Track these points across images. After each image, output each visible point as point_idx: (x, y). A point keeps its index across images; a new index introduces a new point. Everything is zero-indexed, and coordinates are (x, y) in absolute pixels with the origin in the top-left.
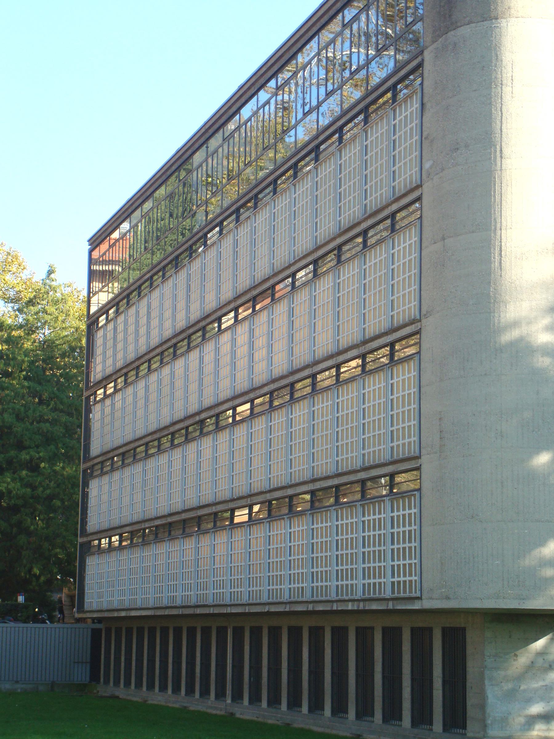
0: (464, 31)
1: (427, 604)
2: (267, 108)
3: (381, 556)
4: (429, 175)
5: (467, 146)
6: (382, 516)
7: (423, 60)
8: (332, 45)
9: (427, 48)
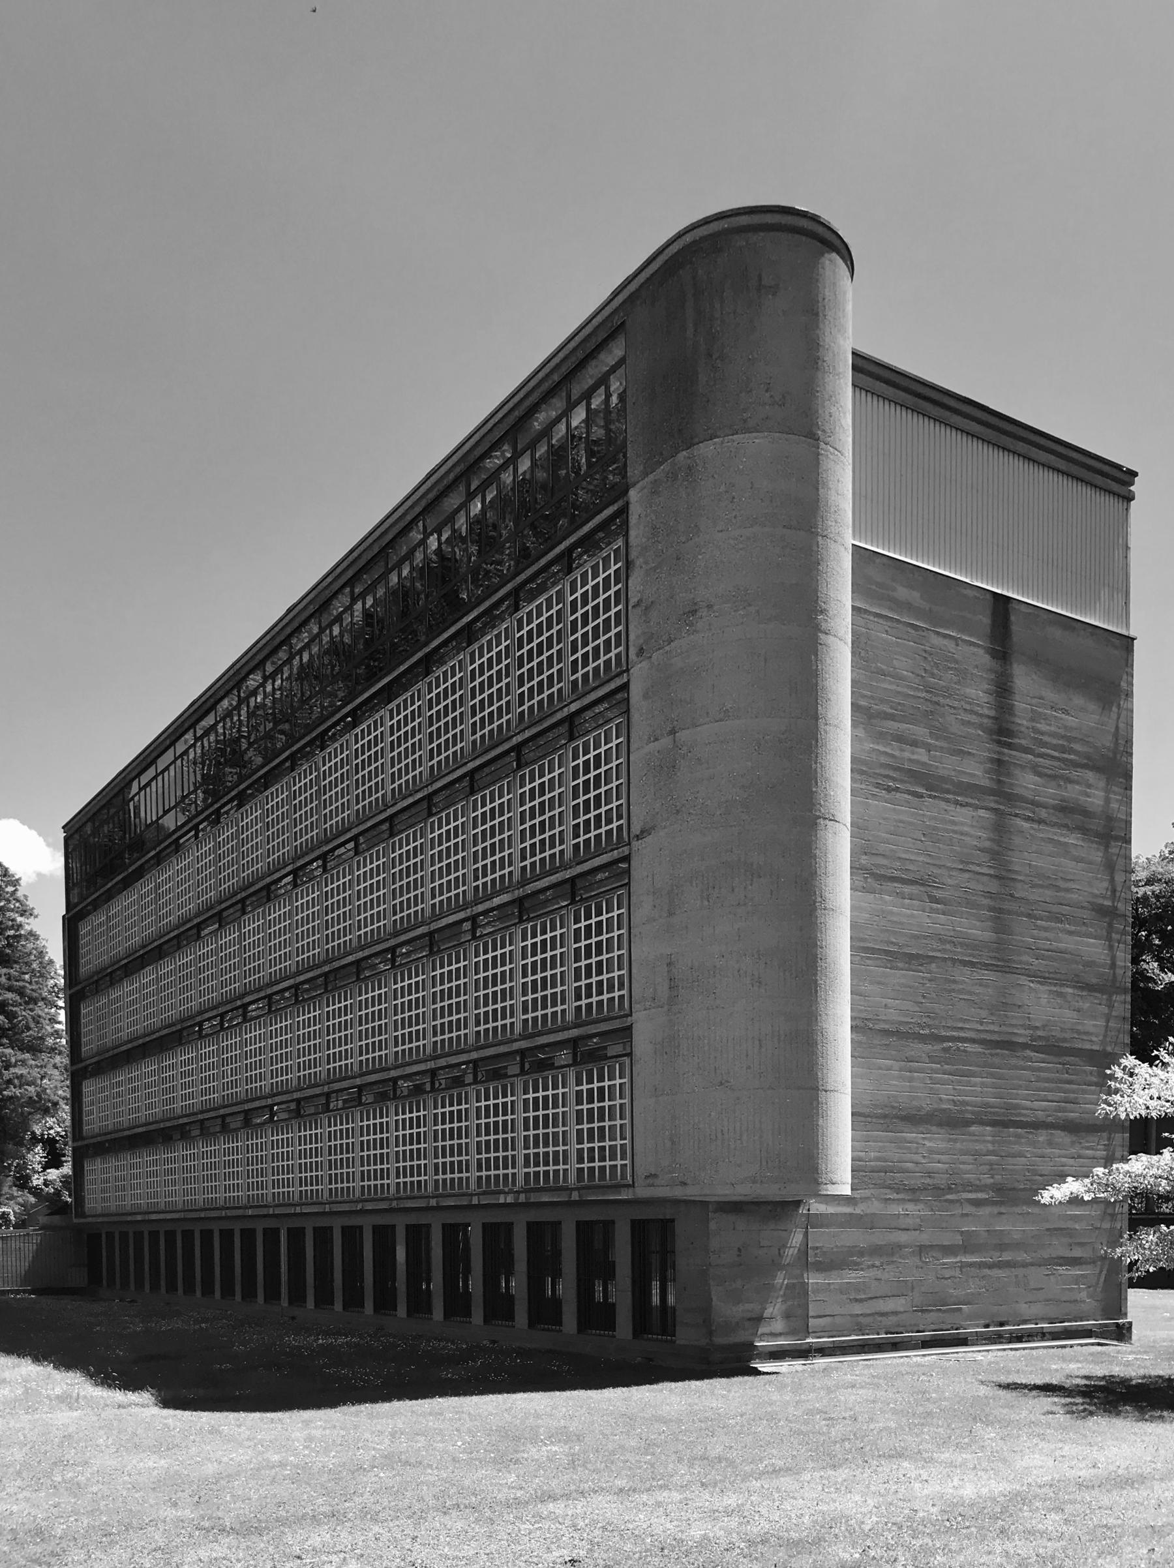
0: (706, 449)
1: (642, 1192)
2: (166, 774)
3: (174, 1183)
4: (641, 652)
5: (710, 607)
6: (350, 1126)
7: (628, 503)
8: (564, 420)
9: (634, 484)
